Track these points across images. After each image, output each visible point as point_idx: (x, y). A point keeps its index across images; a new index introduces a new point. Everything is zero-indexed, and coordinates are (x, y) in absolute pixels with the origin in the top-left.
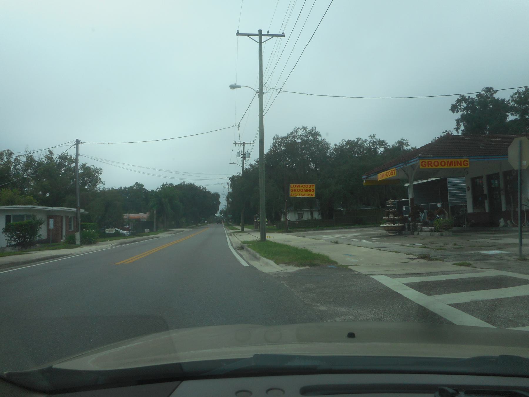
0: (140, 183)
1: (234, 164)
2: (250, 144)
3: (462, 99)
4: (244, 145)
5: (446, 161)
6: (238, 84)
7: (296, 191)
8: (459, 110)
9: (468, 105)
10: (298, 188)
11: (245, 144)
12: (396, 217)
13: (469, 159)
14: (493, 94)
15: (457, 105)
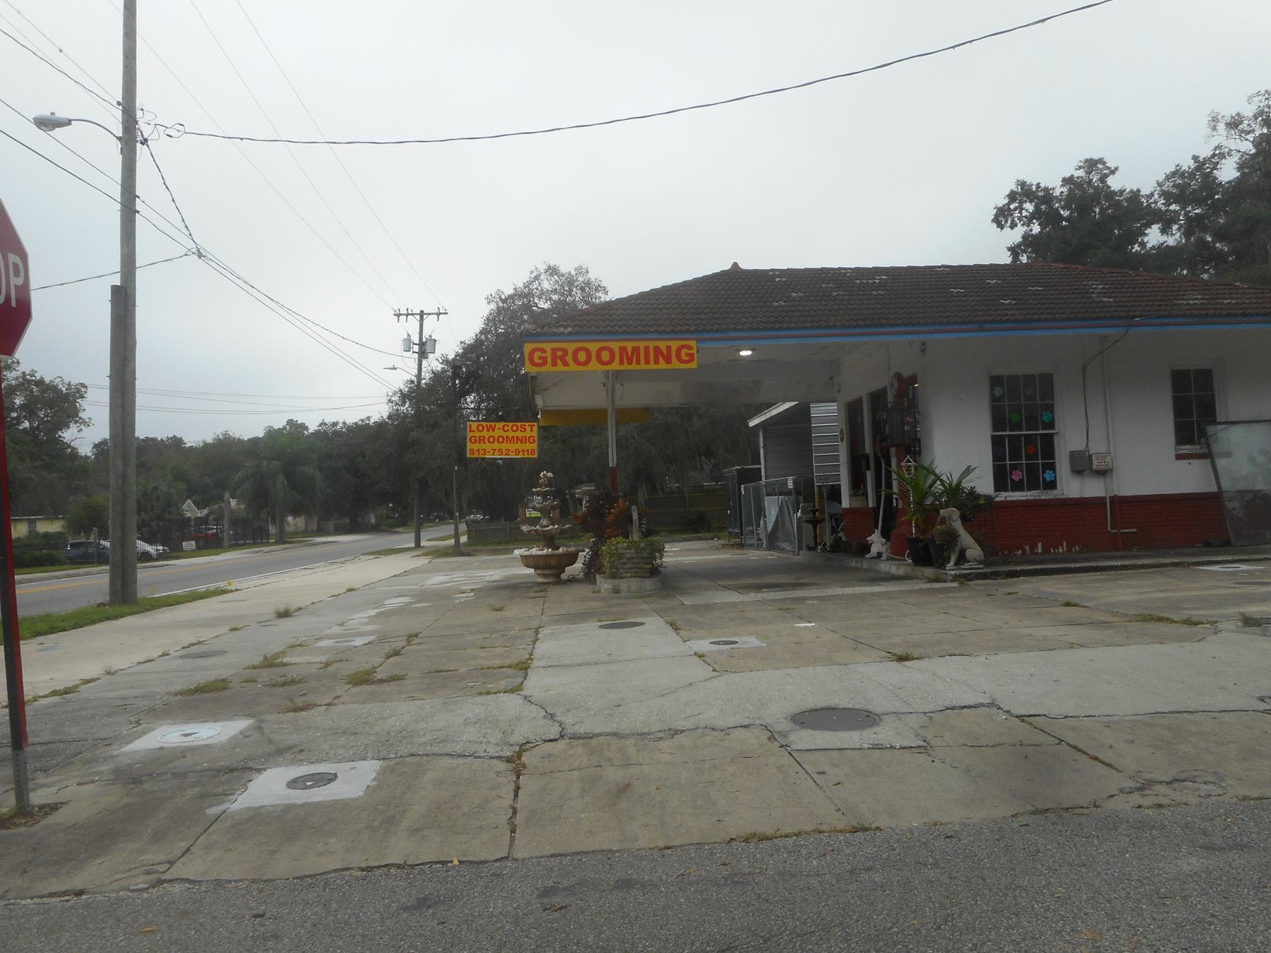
0: (299, 422)
1: (396, 369)
2: (436, 316)
3: (1024, 192)
4: (422, 320)
5: (615, 346)
6: (61, 114)
7: (484, 443)
8: (1018, 222)
9: (1037, 207)
10: (491, 433)
11: (425, 316)
12: (567, 526)
13: (698, 340)
14: (1106, 176)
15: (1012, 207)
